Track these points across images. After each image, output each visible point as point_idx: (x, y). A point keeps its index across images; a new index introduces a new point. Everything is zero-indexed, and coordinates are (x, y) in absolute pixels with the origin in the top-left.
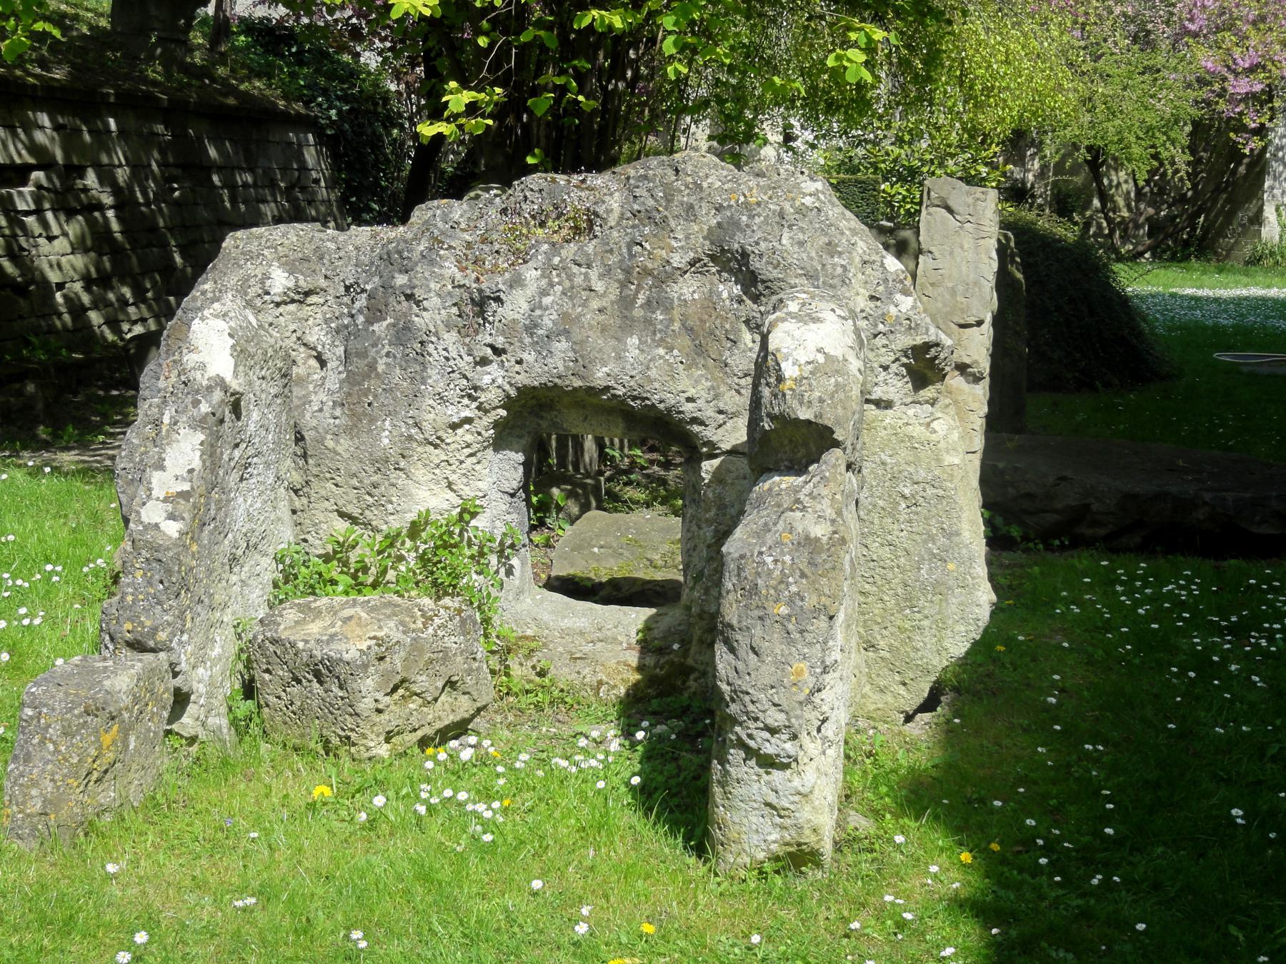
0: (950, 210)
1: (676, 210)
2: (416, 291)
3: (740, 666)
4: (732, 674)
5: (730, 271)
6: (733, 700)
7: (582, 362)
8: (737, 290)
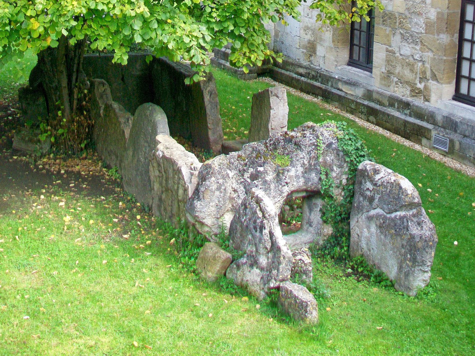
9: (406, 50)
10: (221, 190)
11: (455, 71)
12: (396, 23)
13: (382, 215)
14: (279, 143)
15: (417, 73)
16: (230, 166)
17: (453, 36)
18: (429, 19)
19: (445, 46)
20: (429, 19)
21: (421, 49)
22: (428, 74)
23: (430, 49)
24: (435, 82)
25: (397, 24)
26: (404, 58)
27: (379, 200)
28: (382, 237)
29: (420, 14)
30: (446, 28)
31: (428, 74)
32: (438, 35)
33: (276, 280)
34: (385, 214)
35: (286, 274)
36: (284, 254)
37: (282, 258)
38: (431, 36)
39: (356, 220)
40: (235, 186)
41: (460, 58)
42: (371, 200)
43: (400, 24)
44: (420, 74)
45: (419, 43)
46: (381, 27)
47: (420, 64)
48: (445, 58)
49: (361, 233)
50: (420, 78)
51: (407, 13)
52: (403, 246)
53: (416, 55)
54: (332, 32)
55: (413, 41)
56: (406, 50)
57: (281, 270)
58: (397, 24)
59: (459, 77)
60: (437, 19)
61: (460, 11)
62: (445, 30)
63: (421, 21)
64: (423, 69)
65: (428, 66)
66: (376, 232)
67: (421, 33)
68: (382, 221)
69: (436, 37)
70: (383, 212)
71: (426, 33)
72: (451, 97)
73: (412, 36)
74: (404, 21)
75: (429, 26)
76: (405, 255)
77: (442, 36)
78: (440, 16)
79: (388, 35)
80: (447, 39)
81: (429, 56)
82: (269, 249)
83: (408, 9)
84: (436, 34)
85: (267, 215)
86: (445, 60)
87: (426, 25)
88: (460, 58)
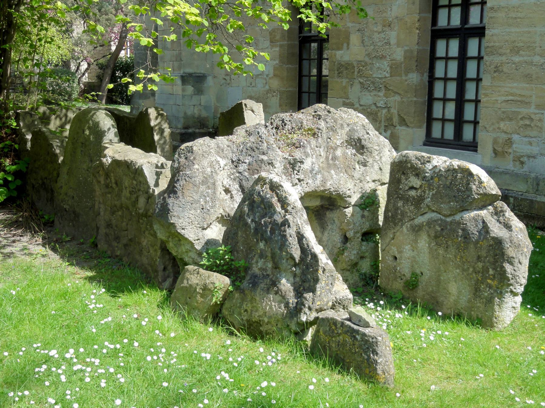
0: (253, 111)
1: (339, 126)
2: (273, 161)
3: (516, 268)
4: (513, 272)
5: (351, 145)
6: (512, 279)
7: (324, 181)
8: (354, 151)
9: (368, 99)
10: (209, 184)
11: (426, 114)
12: (354, 72)
13: (438, 220)
14: (285, 125)
15: (381, 121)
16: (220, 151)
17: (423, 75)
18: (394, 60)
19: (416, 86)
20: (394, 60)
21: (385, 96)
22: (396, 120)
23: (396, 93)
24: (404, 128)
25: (356, 73)
26: (365, 108)
27: (432, 198)
28: (441, 252)
29: (383, 57)
30: (417, 66)
31: (396, 120)
32: (406, 75)
33: (310, 309)
34: (443, 218)
35: (325, 300)
36: (323, 265)
37: (320, 271)
38: (398, 78)
39: (391, 236)
40: (227, 182)
41: (431, 99)
42: (418, 202)
43: (359, 72)
44: (385, 121)
45: (383, 89)
46: (336, 80)
47: (384, 111)
48: (415, 99)
49: (400, 252)
50: (385, 126)
51: (367, 59)
52: (479, 258)
53: (379, 103)
54: (279, 96)
55: (376, 88)
56: (368, 99)
57: (319, 293)
58: (356, 73)
59: (430, 120)
60: (405, 58)
61: (429, 48)
62: (414, 68)
63: (385, 65)
64: (389, 116)
65: (394, 111)
66: (429, 246)
67: (386, 77)
68: (439, 229)
69: (404, 78)
70: (439, 216)
71: (391, 76)
72: (421, 143)
73: (373, 83)
74: (364, 69)
75: (395, 68)
76: (485, 270)
77: (410, 75)
78: (408, 55)
79: (345, 87)
80: (415, 78)
81: (396, 100)
82: (297, 261)
83: (368, 55)
84: (403, 75)
85: (289, 208)
86: (415, 102)
87: (391, 67)
88: (431, 99)
